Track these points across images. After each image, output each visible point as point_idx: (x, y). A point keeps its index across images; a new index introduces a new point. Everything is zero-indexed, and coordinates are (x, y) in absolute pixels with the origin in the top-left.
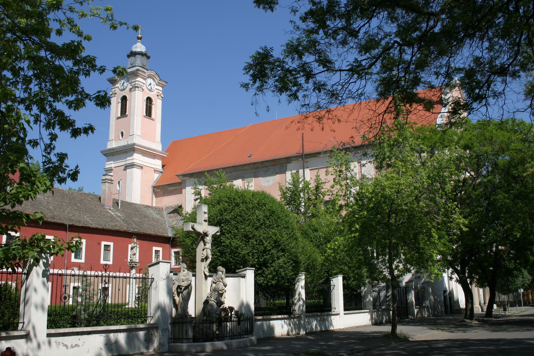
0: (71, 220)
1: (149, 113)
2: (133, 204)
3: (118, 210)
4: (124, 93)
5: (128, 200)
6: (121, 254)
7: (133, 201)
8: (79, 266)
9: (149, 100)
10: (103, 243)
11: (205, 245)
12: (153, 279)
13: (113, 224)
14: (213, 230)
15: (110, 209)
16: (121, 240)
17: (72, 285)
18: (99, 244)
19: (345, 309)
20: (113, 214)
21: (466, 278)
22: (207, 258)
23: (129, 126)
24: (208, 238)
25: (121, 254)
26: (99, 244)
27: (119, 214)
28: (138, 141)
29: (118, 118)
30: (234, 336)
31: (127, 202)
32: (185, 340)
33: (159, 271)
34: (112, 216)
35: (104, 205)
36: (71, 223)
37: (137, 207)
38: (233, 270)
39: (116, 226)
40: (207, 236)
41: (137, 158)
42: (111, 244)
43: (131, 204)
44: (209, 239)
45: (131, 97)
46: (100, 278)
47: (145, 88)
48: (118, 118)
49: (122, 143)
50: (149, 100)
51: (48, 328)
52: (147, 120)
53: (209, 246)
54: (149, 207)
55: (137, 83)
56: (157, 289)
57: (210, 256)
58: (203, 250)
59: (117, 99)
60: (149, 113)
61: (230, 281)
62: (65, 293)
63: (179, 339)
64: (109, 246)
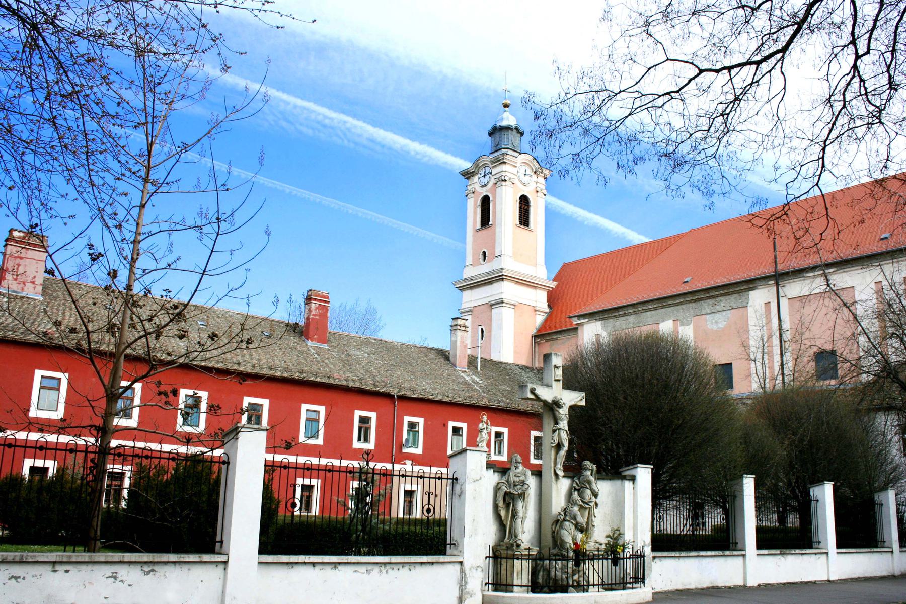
0: (400, 388)
1: (524, 219)
2: (502, 363)
3: (477, 373)
4: (484, 192)
5: (495, 357)
6: (389, 430)
7: (504, 360)
8: (416, 460)
9: (524, 201)
10: (451, 424)
11: (556, 423)
12: (456, 479)
13: (467, 394)
14: (573, 398)
15: (463, 372)
16: (521, 422)
17: (314, 482)
18: (445, 425)
19: (838, 547)
20: (467, 378)
21: (242, 412)
22: (559, 447)
23: (493, 243)
24: (561, 411)
25: (389, 430)
26: (444, 425)
27: (477, 379)
28: (509, 264)
29: (478, 230)
30: (500, 585)
31: (491, 361)
32: (571, 589)
33: (465, 466)
34: (466, 383)
35: (455, 366)
36: (400, 393)
37: (508, 368)
38: (615, 469)
39: (470, 397)
40: (559, 406)
41: (506, 290)
42: (373, 415)
43: (498, 364)
44: (564, 412)
45: (495, 198)
46: (80, 456)
47: (516, 181)
48: (478, 230)
49: (484, 269)
50: (524, 201)
51: (261, 552)
52: (522, 231)
53: (564, 424)
54: (527, 368)
55: (504, 174)
56: (462, 497)
57: (566, 444)
58: (554, 431)
59: (475, 202)
60: (524, 219)
61: (604, 488)
62: (429, 503)
63: (506, 585)
64: (460, 429)
